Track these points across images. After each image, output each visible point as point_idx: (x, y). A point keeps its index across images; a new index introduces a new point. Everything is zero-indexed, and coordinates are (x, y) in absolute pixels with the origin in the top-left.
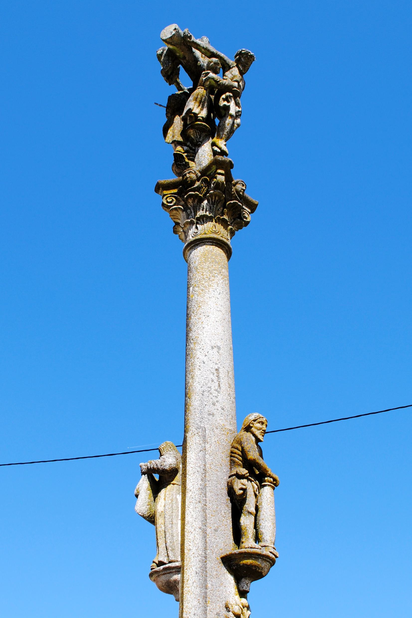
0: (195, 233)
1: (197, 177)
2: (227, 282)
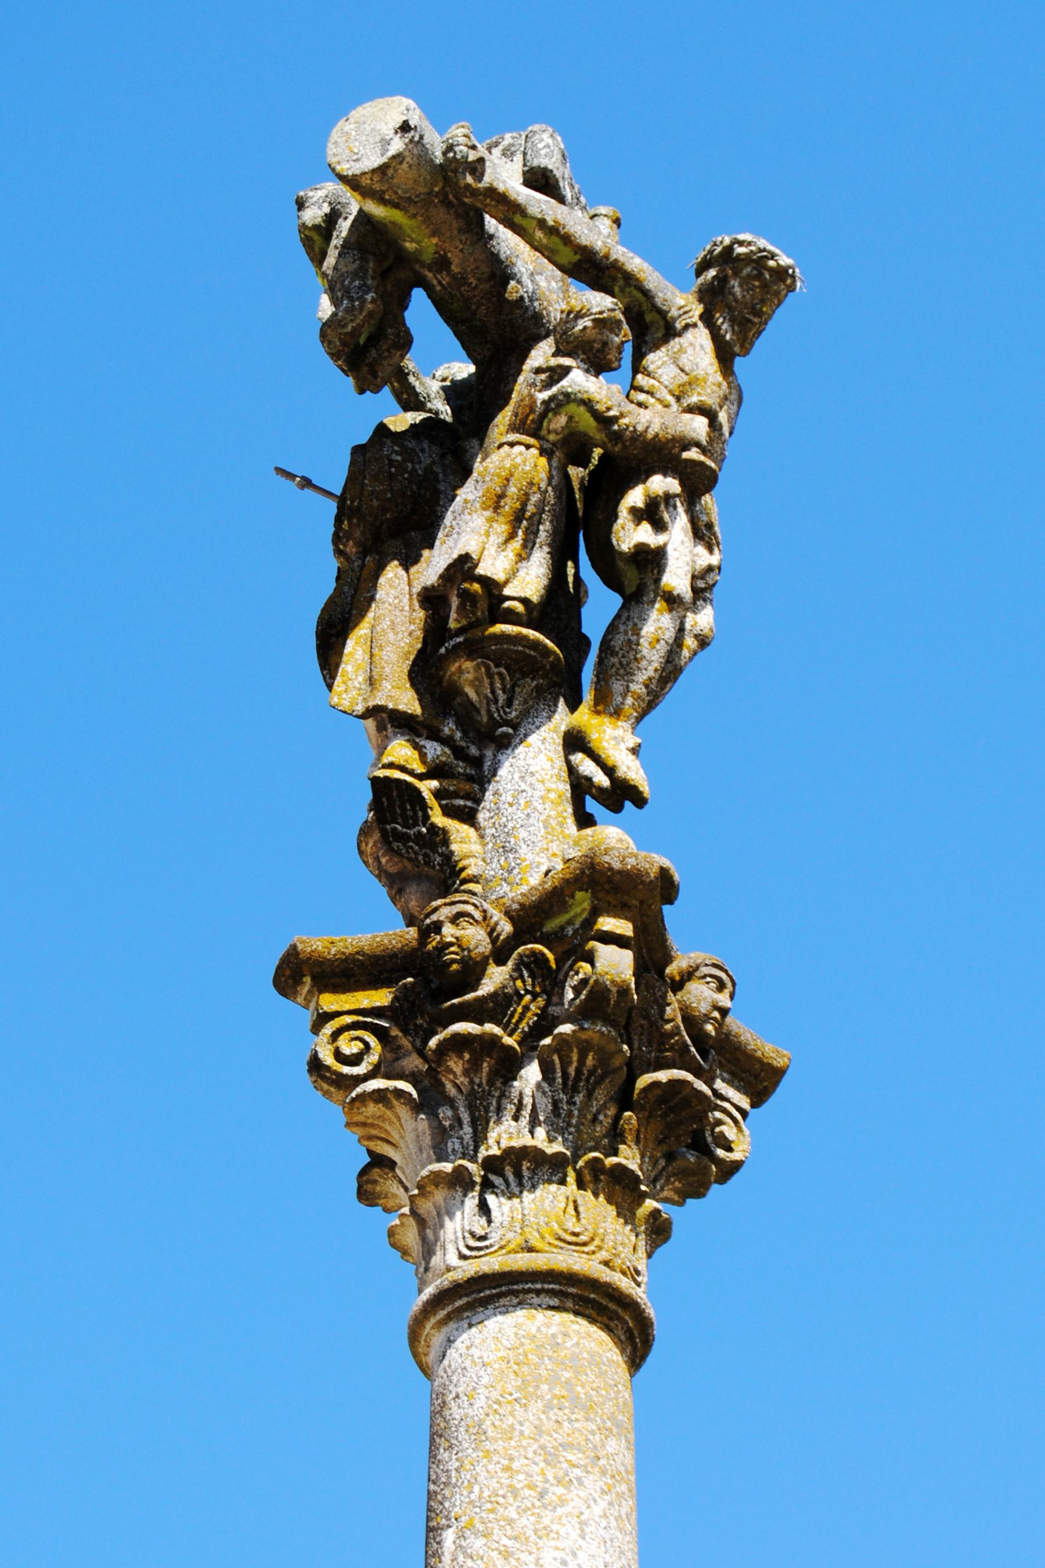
0: (473, 1234)
1: (494, 941)
2: (628, 1505)
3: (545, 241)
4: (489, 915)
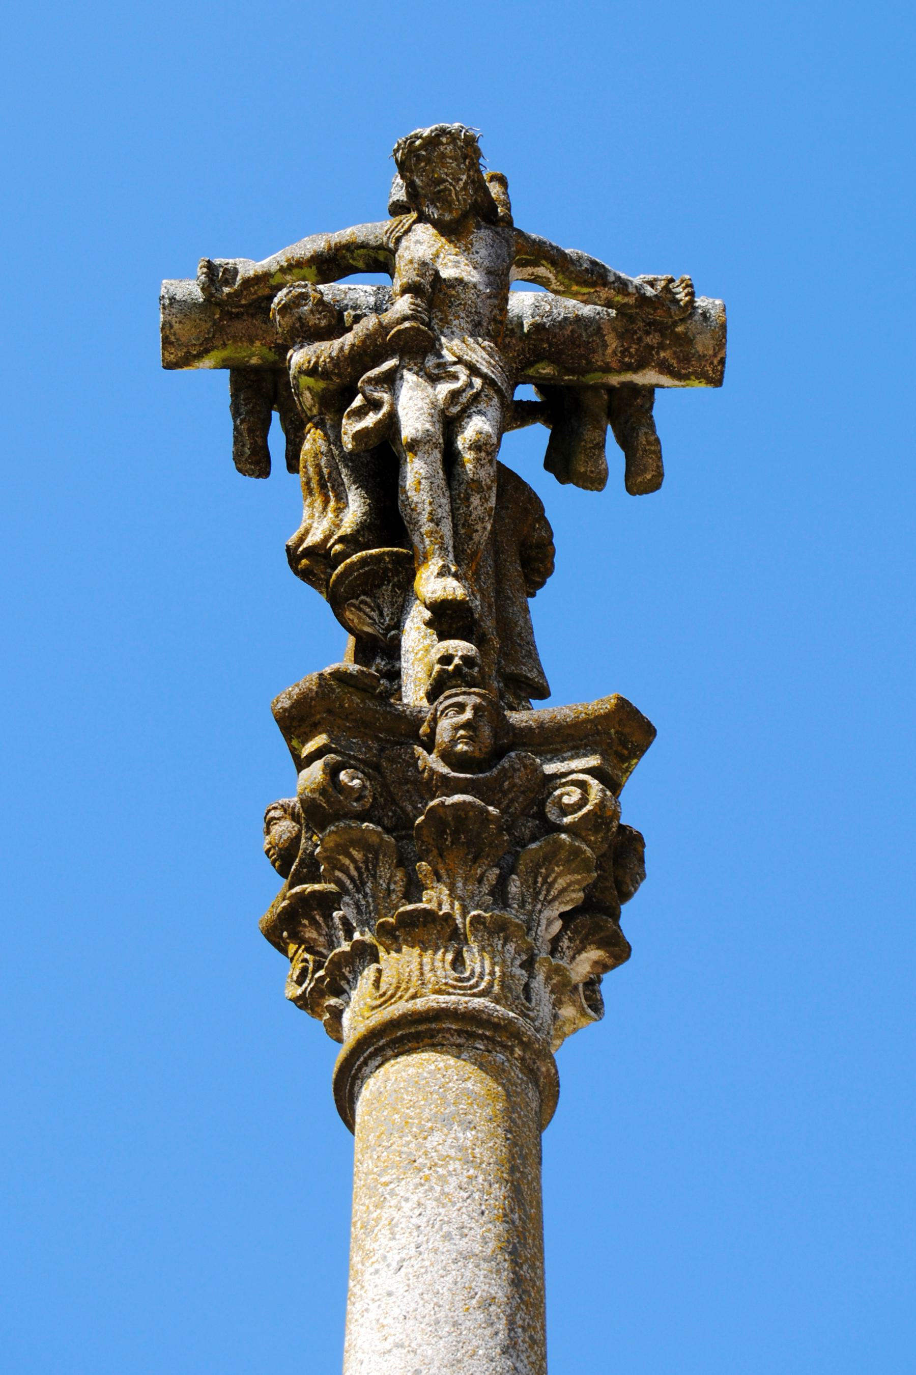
4: (286, 807)
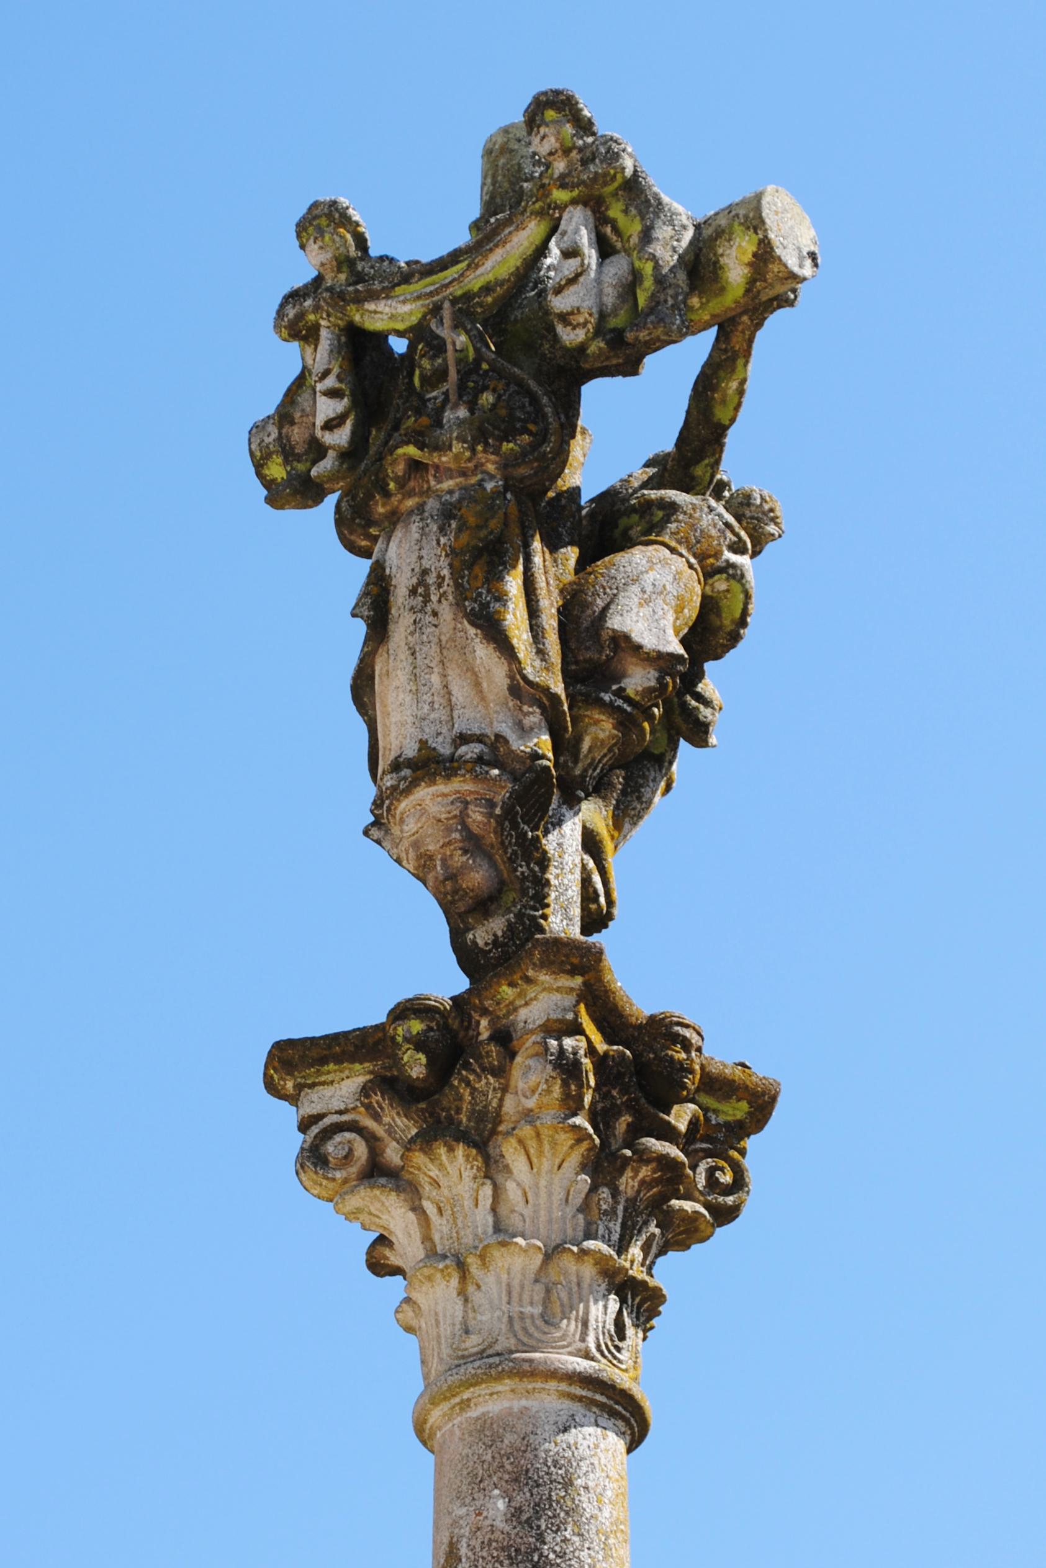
3: (730, 392)
